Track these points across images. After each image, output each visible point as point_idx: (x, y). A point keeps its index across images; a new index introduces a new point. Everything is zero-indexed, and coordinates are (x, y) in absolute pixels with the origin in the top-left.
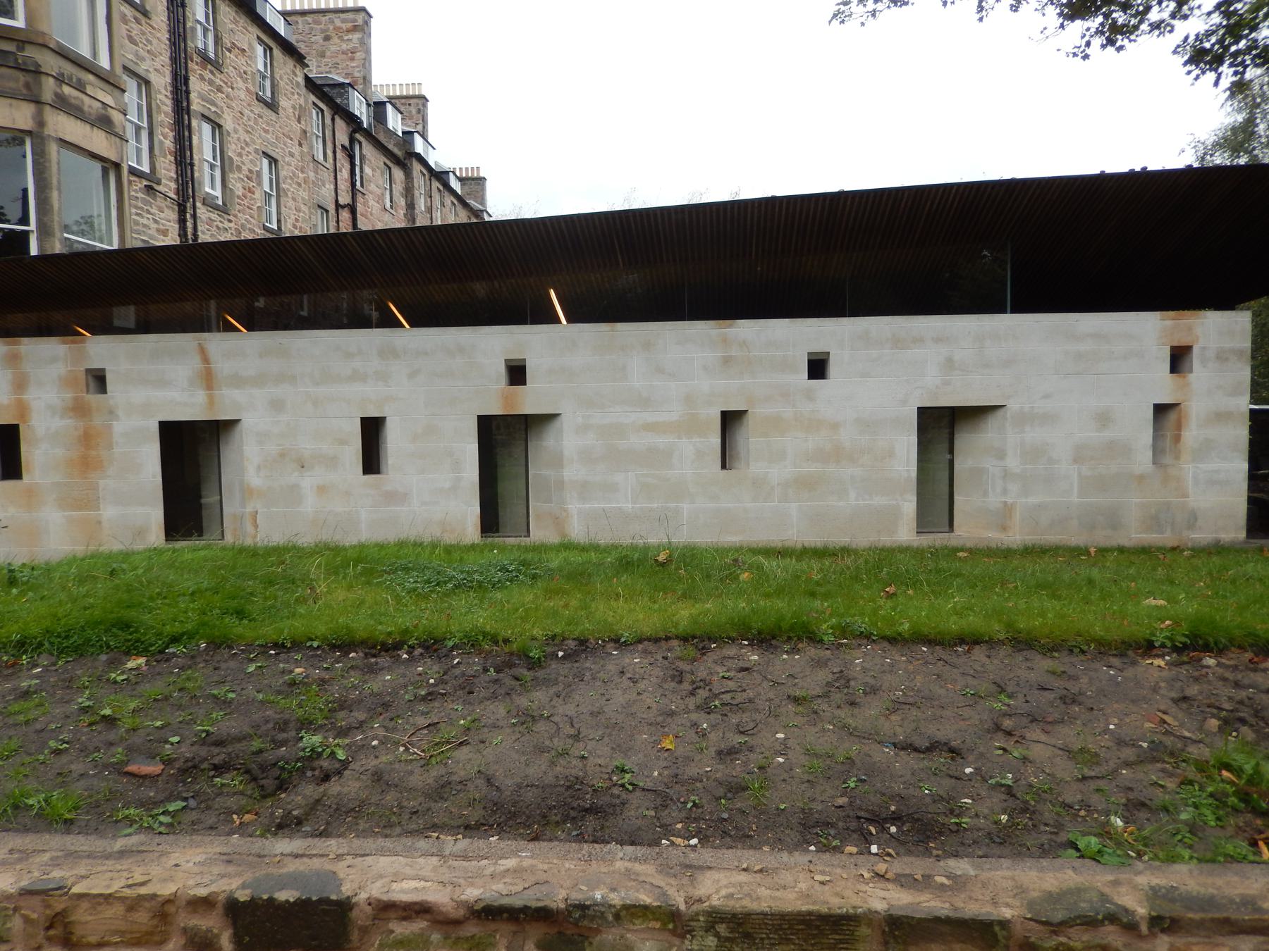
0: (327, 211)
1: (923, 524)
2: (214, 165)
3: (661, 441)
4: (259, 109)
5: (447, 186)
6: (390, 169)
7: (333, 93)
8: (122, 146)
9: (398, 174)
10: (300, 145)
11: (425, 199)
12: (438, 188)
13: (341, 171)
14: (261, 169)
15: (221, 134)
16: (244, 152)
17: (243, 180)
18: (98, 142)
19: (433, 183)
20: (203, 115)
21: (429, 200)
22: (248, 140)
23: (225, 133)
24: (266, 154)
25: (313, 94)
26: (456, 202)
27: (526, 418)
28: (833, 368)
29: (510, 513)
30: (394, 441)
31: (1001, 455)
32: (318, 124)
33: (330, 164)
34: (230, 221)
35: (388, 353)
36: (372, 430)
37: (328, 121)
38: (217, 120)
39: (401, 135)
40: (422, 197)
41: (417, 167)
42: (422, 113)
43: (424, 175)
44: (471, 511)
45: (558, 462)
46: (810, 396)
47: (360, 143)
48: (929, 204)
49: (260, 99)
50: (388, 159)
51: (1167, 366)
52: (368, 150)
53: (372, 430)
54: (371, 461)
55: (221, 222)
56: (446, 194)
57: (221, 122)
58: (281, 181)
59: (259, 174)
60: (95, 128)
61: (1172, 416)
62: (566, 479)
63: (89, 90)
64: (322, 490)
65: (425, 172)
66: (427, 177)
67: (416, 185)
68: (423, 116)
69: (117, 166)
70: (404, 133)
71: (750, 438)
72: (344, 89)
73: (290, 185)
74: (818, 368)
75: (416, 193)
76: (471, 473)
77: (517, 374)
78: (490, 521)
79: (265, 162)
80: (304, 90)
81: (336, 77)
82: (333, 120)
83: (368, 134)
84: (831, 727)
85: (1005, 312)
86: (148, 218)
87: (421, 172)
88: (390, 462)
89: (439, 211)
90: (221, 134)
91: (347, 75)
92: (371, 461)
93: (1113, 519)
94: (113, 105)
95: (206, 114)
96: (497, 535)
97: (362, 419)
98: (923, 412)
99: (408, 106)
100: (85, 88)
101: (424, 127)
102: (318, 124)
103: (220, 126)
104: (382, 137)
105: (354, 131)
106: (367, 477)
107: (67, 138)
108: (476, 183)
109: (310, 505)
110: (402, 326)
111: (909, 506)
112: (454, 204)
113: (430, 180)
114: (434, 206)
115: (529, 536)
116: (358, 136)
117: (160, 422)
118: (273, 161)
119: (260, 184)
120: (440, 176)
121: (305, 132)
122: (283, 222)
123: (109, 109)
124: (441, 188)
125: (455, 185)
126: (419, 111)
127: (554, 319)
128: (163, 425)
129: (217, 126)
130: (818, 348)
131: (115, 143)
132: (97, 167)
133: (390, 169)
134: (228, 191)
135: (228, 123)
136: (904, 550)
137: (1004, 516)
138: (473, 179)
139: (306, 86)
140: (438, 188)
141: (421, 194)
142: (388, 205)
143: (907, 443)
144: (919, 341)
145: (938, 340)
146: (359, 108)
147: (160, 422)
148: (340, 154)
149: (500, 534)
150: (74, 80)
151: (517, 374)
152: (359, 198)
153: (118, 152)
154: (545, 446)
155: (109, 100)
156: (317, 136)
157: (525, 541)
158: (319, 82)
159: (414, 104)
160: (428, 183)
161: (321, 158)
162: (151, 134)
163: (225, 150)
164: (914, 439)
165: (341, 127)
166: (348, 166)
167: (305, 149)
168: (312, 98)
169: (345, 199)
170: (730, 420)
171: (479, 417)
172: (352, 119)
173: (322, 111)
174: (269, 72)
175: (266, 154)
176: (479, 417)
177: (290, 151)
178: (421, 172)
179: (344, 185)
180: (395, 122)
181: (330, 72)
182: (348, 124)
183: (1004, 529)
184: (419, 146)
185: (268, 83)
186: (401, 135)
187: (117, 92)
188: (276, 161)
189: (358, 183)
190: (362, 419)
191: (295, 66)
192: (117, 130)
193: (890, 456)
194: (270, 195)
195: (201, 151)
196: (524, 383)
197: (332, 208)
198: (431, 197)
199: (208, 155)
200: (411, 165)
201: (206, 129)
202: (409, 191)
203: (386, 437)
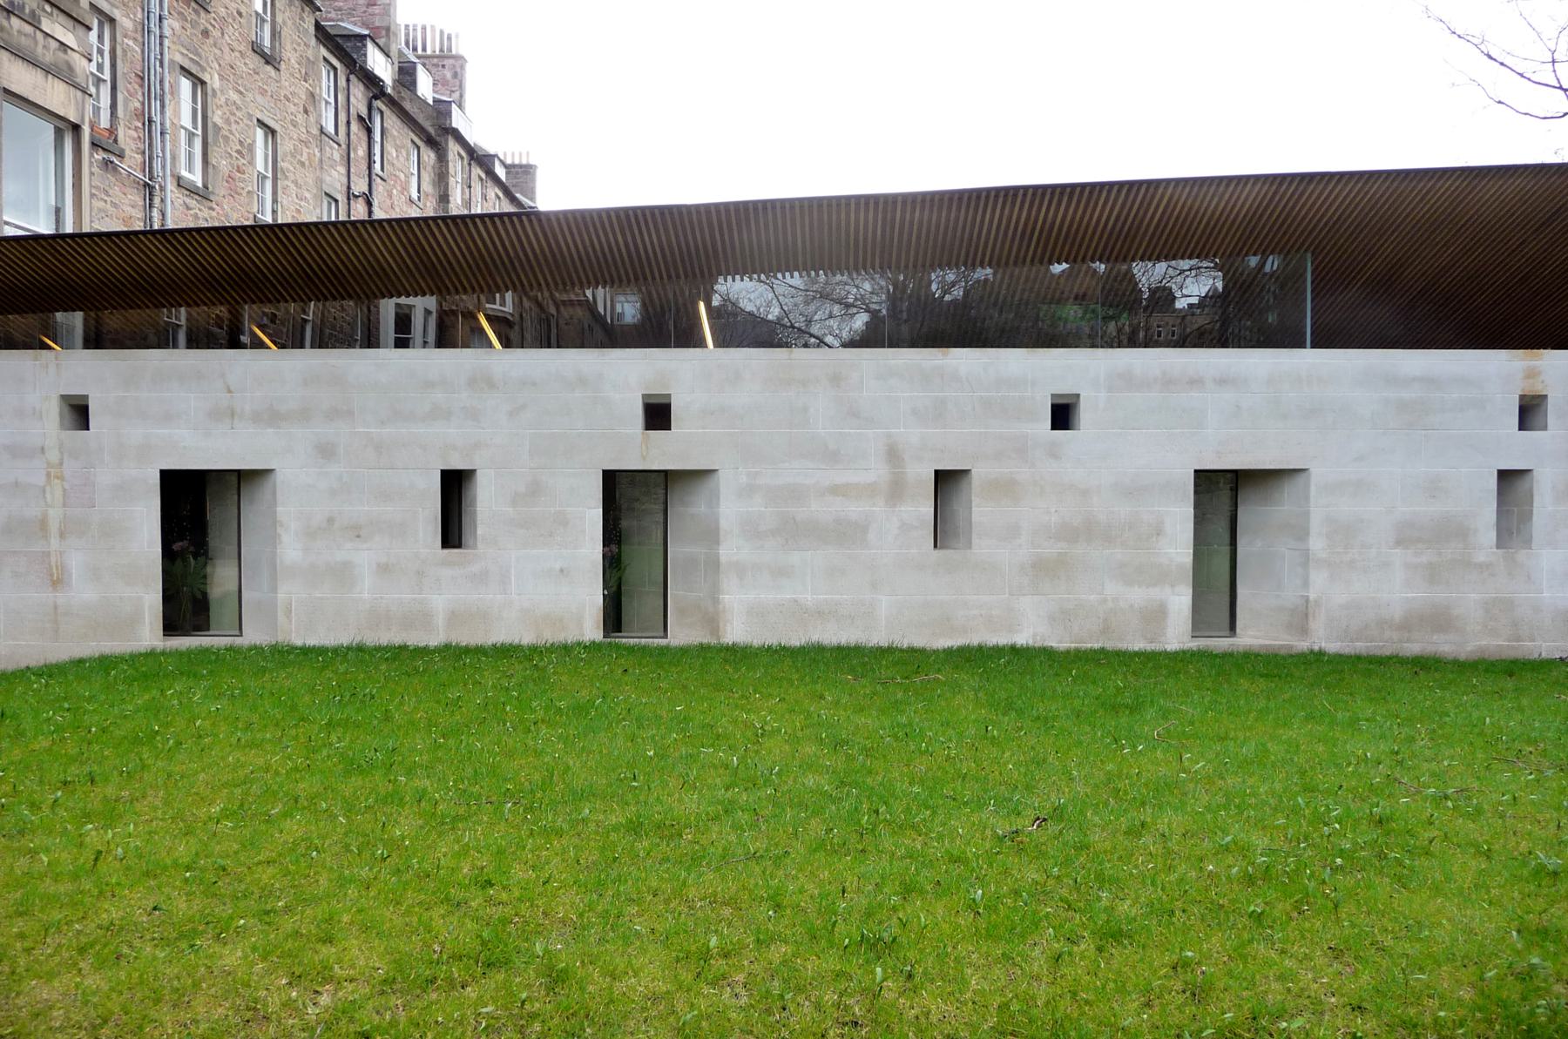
0: (336, 201)
1: (1200, 622)
2: (193, 134)
3: (854, 509)
4: (254, 61)
5: (490, 173)
6: (418, 148)
7: (348, 45)
8: (83, 102)
9: (429, 156)
10: (306, 111)
11: (463, 189)
12: (479, 176)
13: (356, 151)
14: (254, 141)
15: (205, 94)
16: (232, 119)
17: (231, 155)
18: (56, 96)
19: (473, 169)
20: (182, 68)
21: (467, 191)
22: (239, 102)
23: (209, 92)
24: (261, 123)
25: (325, 46)
26: (501, 195)
27: (666, 475)
28: (1084, 414)
29: (639, 607)
30: (485, 500)
31: (1302, 534)
32: (329, 87)
33: (342, 137)
34: (211, 209)
35: (482, 382)
36: (455, 485)
37: (342, 82)
38: (200, 75)
39: (431, 103)
40: (459, 186)
41: (453, 148)
42: (459, 76)
43: (462, 158)
44: (592, 596)
45: (712, 535)
46: (1054, 453)
47: (382, 113)
48: (1216, 200)
49: (257, 49)
50: (417, 135)
51: (1515, 420)
52: (392, 122)
53: (455, 485)
54: (452, 532)
55: (200, 210)
56: (490, 184)
57: (206, 77)
58: (279, 159)
59: (251, 148)
60: (50, 76)
61: (1521, 485)
62: (723, 559)
63: (46, 25)
64: (384, 569)
65: (463, 154)
66: (466, 162)
67: (451, 170)
68: (461, 82)
69: (76, 128)
70: (435, 101)
71: (979, 509)
72: (361, 41)
73: (291, 163)
74: (1063, 415)
75: (452, 181)
76: (592, 549)
77: (658, 415)
78: (614, 617)
79: (260, 133)
80: (313, 41)
81: (350, 27)
82: (348, 80)
83: (393, 103)
84: (91, 826)
85: (1301, 345)
86: (106, 201)
87: (459, 154)
88: (479, 532)
89: (479, 205)
90: (205, 94)
91: (365, 25)
92: (452, 532)
93: (1440, 619)
94: (76, 48)
95: (186, 67)
96: (619, 634)
97: (443, 472)
98: (1200, 474)
99: (440, 68)
100: (40, 22)
101: (461, 96)
102: (329, 87)
103: (203, 83)
104: (407, 106)
105: (376, 97)
106: (446, 551)
107: (14, 88)
108: (523, 172)
109: (366, 590)
110: (490, 345)
111: (1180, 601)
112: (499, 198)
113: (470, 164)
114: (473, 199)
115: (666, 636)
116: (378, 104)
117: (162, 472)
118: (270, 132)
119: (252, 162)
120: (480, 159)
121: (312, 95)
122: (279, 213)
123: (69, 51)
124: (483, 176)
125: (500, 172)
126: (455, 75)
127: (701, 343)
128: (165, 475)
129: (198, 82)
130: (1065, 388)
131: (75, 97)
132: (48, 130)
133: (418, 148)
134: (210, 170)
135: (214, 80)
136: (151, 654)
137: (1301, 617)
138: (521, 166)
139: (316, 36)
140: (479, 176)
141: (457, 182)
142: (415, 195)
143: (1180, 517)
144: (1196, 382)
145: (1223, 382)
146: (379, 64)
147: (162, 472)
148: (354, 127)
149: (211, 633)
150: (27, 11)
151: (658, 415)
152: (379, 186)
153: (78, 109)
154: (687, 511)
155: (69, 40)
156: (327, 102)
157: (238, 641)
158: (332, 32)
159: (448, 64)
160: (468, 168)
161: (331, 129)
162: (114, 88)
163: (210, 114)
164: (1188, 510)
165: (359, 95)
166: (365, 145)
167: (312, 119)
168: (324, 52)
169: (360, 186)
170: (946, 481)
171: (604, 471)
172: (371, 80)
173: (335, 69)
174: (269, 14)
175: (261, 123)
176: (604, 471)
177: (292, 120)
178: (459, 154)
179: (359, 166)
180: (425, 86)
181: (342, 20)
182: (367, 87)
183: (1304, 631)
184: (457, 121)
185: (267, 28)
186: (431, 103)
187: (81, 30)
188: (273, 132)
189: (377, 166)
190: (443, 472)
191: (303, 10)
192: (78, 80)
193: (1158, 534)
194: (265, 177)
195: (177, 113)
196: (668, 428)
197: (341, 198)
198: (470, 187)
199: (186, 121)
200: (447, 144)
201: (185, 85)
202: (442, 178)
203: (474, 499)
